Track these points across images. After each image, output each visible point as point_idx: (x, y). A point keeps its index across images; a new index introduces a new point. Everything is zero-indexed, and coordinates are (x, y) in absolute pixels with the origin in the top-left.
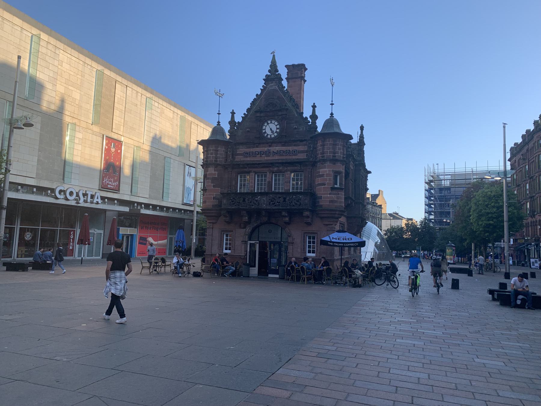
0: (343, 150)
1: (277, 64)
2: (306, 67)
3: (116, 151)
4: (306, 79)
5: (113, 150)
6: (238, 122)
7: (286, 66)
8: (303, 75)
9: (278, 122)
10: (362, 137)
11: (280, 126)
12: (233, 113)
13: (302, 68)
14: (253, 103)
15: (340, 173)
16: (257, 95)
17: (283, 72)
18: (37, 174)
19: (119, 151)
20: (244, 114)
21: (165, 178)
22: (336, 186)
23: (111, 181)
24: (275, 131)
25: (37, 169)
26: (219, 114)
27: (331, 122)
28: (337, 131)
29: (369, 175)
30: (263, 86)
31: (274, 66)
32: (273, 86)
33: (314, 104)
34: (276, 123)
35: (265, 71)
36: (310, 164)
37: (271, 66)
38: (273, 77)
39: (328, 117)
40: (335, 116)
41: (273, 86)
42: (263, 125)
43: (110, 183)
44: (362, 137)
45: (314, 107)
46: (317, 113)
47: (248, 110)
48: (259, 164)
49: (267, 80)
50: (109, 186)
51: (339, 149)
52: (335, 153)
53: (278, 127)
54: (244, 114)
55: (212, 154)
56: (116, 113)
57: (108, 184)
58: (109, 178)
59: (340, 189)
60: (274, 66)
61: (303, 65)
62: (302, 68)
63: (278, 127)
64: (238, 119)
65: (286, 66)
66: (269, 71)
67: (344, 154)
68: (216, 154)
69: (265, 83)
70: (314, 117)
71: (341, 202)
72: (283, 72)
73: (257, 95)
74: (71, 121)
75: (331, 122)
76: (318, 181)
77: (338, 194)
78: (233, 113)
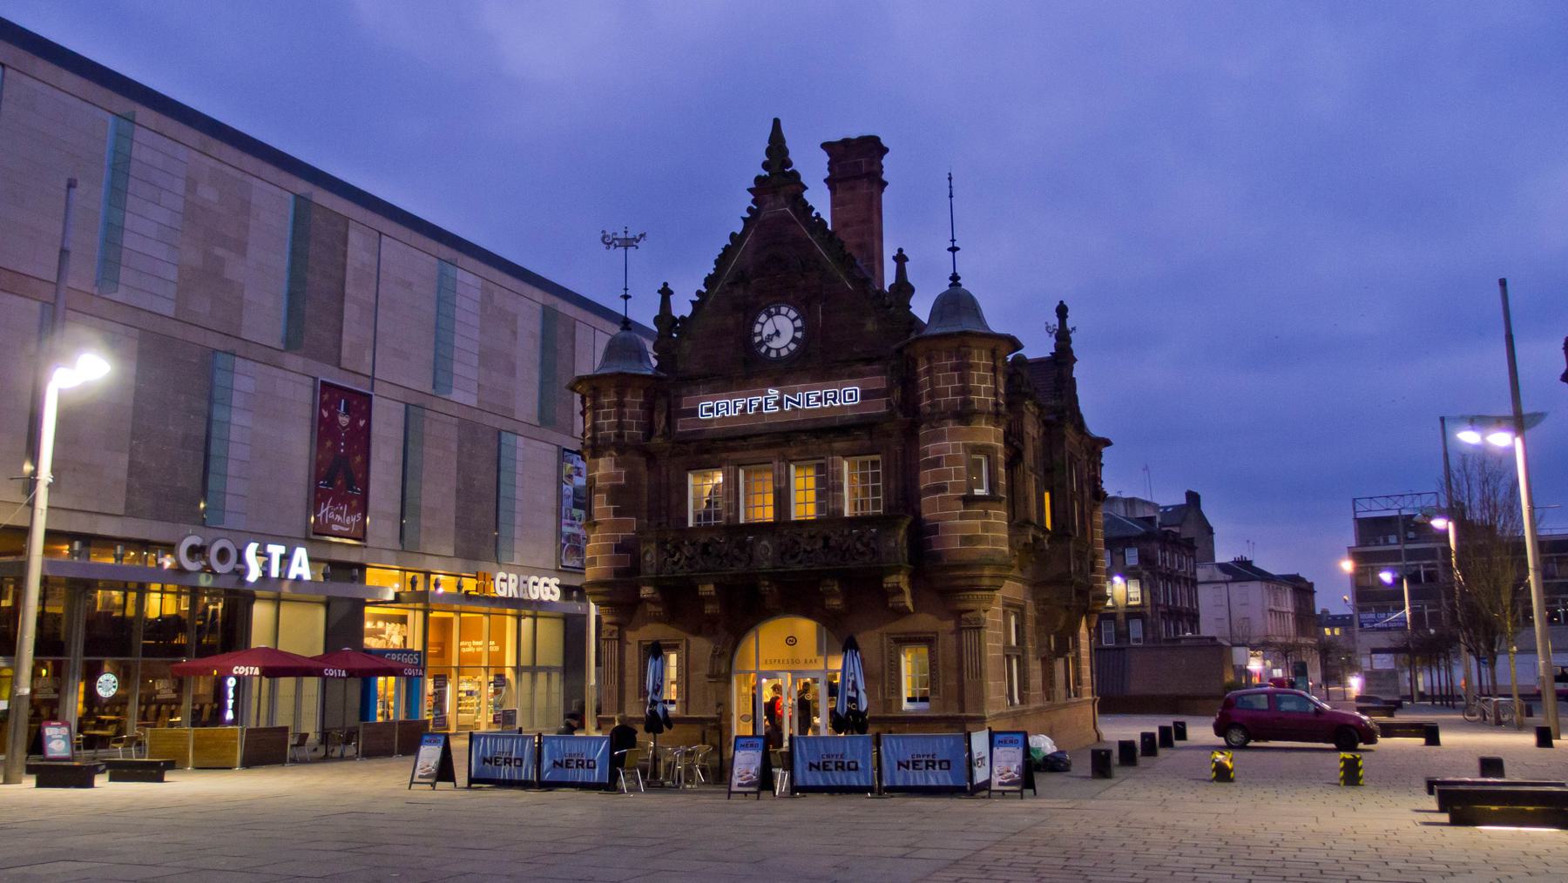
0: (995, 382)
1: (788, 145)
2: (885, 142)
3: (353, 423)
4: (885, 177)
5: (344, 420)
6: (682, 317)
7: (825, 146)
8: (875, 168)
9: (797, 308)
10: (1063, 336)
11: (804, 320)
12: (666, 293)
13: (872, 148)
14: (722, 261)
15: (987, 450)
16: (733, 236)
17: (812, 168)
18: (128, 505)
19: (362, 423)
20: (699, 293)
21: (502, 493)
22: (977, 492)
23: (341, 513)
24: (771, 345)
25: (130, 489)
26: (626, 297)
27: (956, 301)
28: (973, 327)
29: (1105, 451)
30: (750, 210)
31: (777, 147)
32: (779, 207)
33: (900, 250)
34: (793, 314)
35: (754, 164)
36: (894, 435)
37: (769, 152)
38: (778, 177)
39: (945, 286)
40: (966, 284)
41: (779, 207)
42: (754, 321)
43: (338, 518)
44: (1063, 336)
45: (901, 259)
46: (911, 278)
47: (710, 281)
48: (744, 438)
49: (761, 188)
50: (335, 528)
51: (982, 380)
52: (970, 392)
53: (799, 323)
54: (699, 293)
55: (607, 416)
56: (351, 311)
57: (332, 521)
58: (334, 504)
59: (992, 499)
60: (777, 147)
61: (874, 140)
62: (872, 148)
63: (799, 323)
64: (682, 308)
65: (825, 146)
66: (765, 166)
67: (996, 394)
68: (620, 415)
69: (754, 202)
70: (904, 288)
71: (995, 541)
72: (812, 168)
73: (733, 236)
74: (221, 347)
75: (956, 301)
76: (926, 478)
77: (987, 515)
78: (666, 293)
